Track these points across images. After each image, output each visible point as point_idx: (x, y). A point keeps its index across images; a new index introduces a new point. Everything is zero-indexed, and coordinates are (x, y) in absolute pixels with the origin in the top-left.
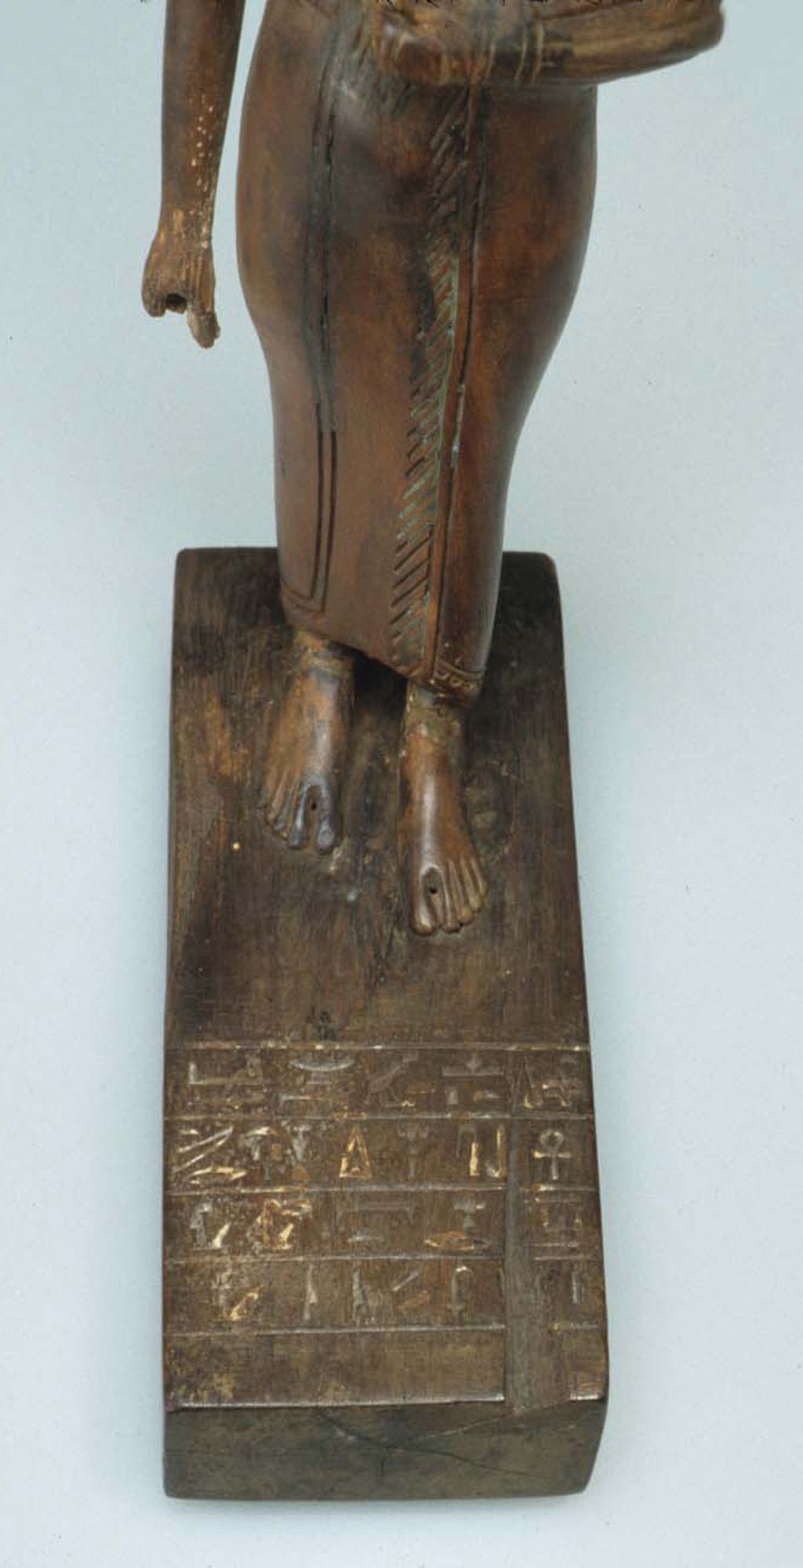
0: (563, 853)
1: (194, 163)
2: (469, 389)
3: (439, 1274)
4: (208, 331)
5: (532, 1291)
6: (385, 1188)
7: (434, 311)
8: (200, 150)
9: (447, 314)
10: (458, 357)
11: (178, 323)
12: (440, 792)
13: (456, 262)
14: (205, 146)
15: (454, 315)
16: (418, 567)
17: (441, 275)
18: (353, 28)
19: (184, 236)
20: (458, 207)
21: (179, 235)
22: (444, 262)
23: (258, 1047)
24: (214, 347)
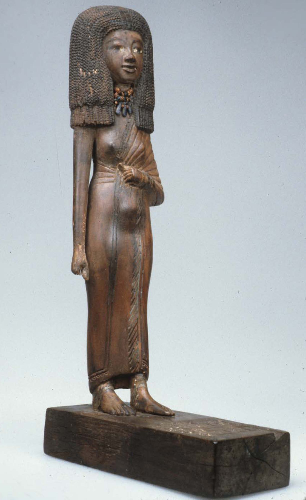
13: (140, 236)
21: (81, 251)
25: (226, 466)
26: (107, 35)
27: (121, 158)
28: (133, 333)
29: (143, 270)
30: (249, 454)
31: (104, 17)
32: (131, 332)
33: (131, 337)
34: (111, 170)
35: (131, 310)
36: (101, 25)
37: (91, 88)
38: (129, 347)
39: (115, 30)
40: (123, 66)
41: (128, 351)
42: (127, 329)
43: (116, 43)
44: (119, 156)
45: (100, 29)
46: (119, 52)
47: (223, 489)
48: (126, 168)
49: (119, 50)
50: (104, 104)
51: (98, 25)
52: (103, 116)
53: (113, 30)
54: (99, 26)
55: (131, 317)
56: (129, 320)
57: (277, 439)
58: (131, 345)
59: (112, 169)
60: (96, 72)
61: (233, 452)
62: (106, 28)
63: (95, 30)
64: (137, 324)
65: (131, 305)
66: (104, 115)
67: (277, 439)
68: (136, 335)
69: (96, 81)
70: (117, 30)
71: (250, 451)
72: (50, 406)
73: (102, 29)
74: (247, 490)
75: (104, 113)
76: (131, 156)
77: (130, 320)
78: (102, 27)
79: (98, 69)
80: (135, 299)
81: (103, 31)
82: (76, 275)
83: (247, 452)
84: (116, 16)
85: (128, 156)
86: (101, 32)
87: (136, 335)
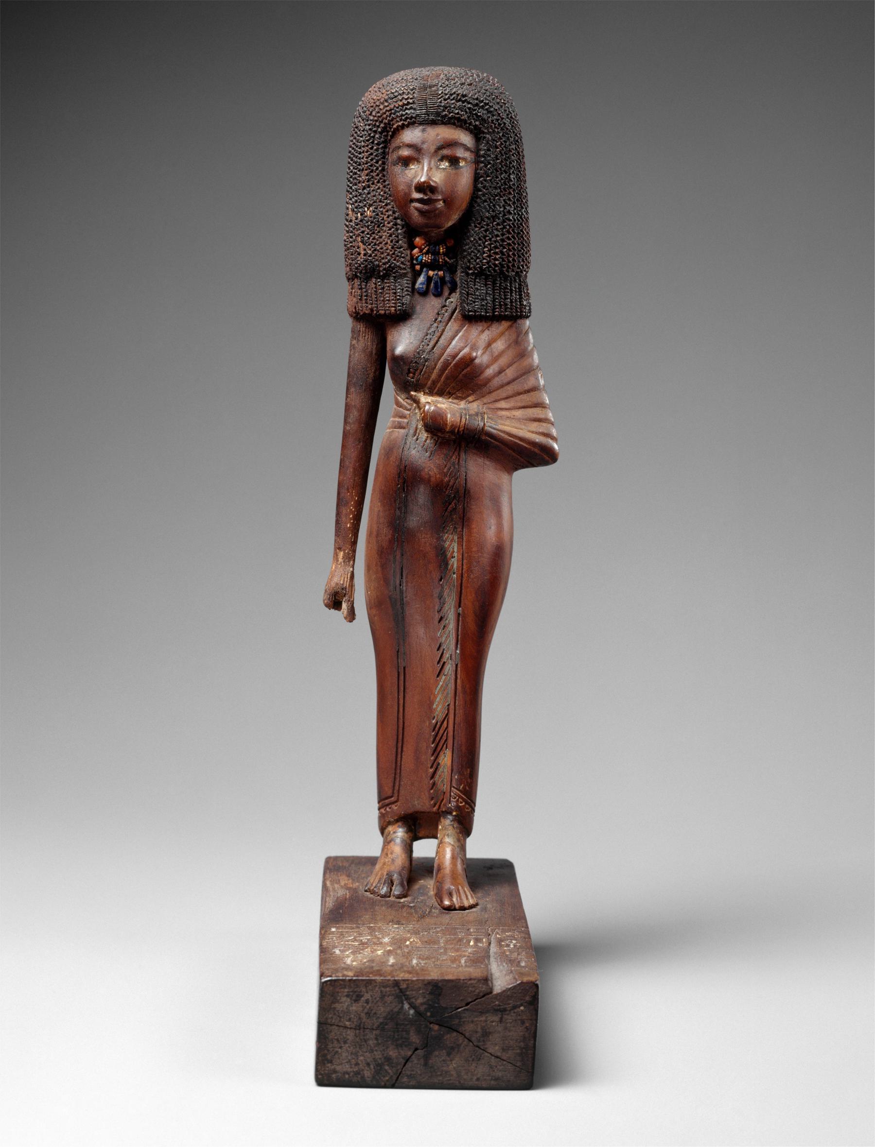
0: (368, 1074)
1: (348, 526)
2: (463, 611)
3: (427, 1041)
4: (351, 616)
5: (425, 1000)
6: (463, 373)
7: (447, 564)
8: (351, 519)
9: (453, 566)
10: (458, 589)
11: (338, 616)
12: (444, 857)
13: (456, 538)
14: (353, 517)
15: (455, 566)
16: (456, 309)
17: (450, 545)
18: (415, 426)
19: (343, 564)
20: (456, 506)
21: (341, 563)
22: (451, 538)
23: (331, 1045)
24: (353, 623)
25: (346, 1027)
26: (392, 137)
27: (418, 381)
28: (441, 732)
29: (460, 606)
30: (412, 1012)
31: (386, 101)
32: (437, 729)
33: (438, 739)
34: (405, 403)
35: (437, 687)
36: (380, 119)
37: (360, 244)
38: (432, 758)
39: (403, 127)
40: (413, 200)
41: (429, 766)
42: (430, 723)
43: (406, 152)
44: (413, 378)
45: (378, 127)
46: (407, 172)
47: (338, 1068)
48: (423, 398)
49: (408, 168)
50: (386, 273)
51: (376, 118)
52: (384, 298)
53: (400, 128)
54: (376, 121)
55: (438, 699)
56: (435, 706)
57: (495, 992)
58: (435, 754)
59: (406, 402)
60: (370, 211)
61: (367, 1002)
62: (389, 124)
63: (370, 129)
64: (447, 715)
65: (438, 676)
66: (387, 295)
67: (495, 992)
68: (444, 738)
69: (369, 231)
70: (408, 126)
71: (412, 1006)
72: (334, 853)
73: (382, 125)
74: (405, 1079)
75: (388, 292)
76: (440, 376)
77: (436, 705)
78: (381, 122)
79: (373, 207)
80: (446, 664)
81: (384, 130)
82: (336, 611)
83: (406, 1006)
84: (406, 99)
85: (434, 376)
86: (381, 133)
87: (444, 738)
